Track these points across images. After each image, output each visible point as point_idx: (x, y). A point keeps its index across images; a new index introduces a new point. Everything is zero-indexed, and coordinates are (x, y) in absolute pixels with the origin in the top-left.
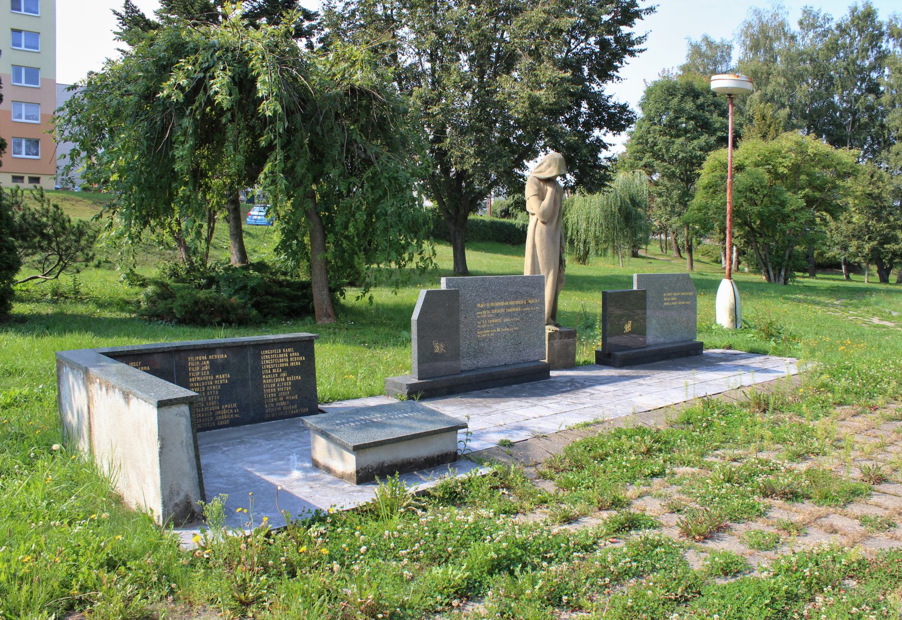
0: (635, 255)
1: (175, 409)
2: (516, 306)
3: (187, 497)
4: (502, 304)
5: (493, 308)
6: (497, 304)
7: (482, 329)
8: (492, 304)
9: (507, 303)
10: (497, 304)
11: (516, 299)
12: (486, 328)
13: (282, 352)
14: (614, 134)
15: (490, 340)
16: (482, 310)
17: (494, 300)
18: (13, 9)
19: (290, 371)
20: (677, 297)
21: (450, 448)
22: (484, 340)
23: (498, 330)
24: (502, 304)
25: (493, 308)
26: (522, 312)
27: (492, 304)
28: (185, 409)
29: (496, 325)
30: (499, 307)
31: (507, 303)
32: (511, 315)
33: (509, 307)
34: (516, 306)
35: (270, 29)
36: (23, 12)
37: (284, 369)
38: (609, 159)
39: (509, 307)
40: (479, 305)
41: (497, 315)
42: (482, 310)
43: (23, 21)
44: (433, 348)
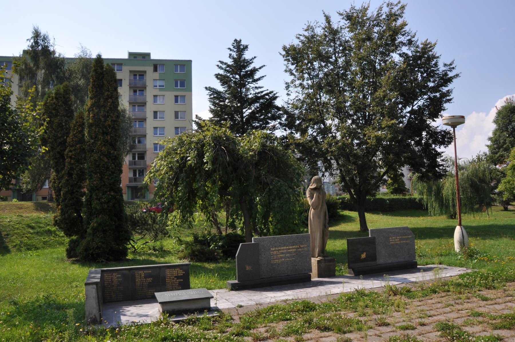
0: (506, 209)
1: (91, 286)
2: (293, 249)
3: (95, 315)
4: (285, 248)
5: (280, 250)
6: (282, 248)
7: (274, 260)
8: (279, 248)
9: (288, 248)
10: (282, 248)
11: (292, 245)
12: (276, 259)
13: (397, 239)
14: (445, 147)
15: (279, 264)
16: (273, 251)
17: (280, 246)
18: (154, 118)
19: (178, 277)
20: (400, 239)
21: (206, 305)
22: (275, 264)
23: (283, 260)
24: (285, 248)
25: (280, 250)
26: (297, 251)
27: (279, 248)
28: (95, 286)
29: (282, 258)
30: (283, 249)
31: (288, 248)
32: (290, 253)
33: (289, 249)
34: (293, 249)
35: (228, 132)
36: (179, 103)
37: (175, 277)
38: (443, 160)
39: (289, 249)
40: (272, 249)
41: (282, 253)
42: (273, 251)
43: (178, 107)
44: (245, 268)
